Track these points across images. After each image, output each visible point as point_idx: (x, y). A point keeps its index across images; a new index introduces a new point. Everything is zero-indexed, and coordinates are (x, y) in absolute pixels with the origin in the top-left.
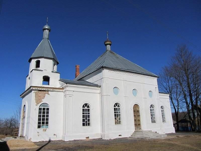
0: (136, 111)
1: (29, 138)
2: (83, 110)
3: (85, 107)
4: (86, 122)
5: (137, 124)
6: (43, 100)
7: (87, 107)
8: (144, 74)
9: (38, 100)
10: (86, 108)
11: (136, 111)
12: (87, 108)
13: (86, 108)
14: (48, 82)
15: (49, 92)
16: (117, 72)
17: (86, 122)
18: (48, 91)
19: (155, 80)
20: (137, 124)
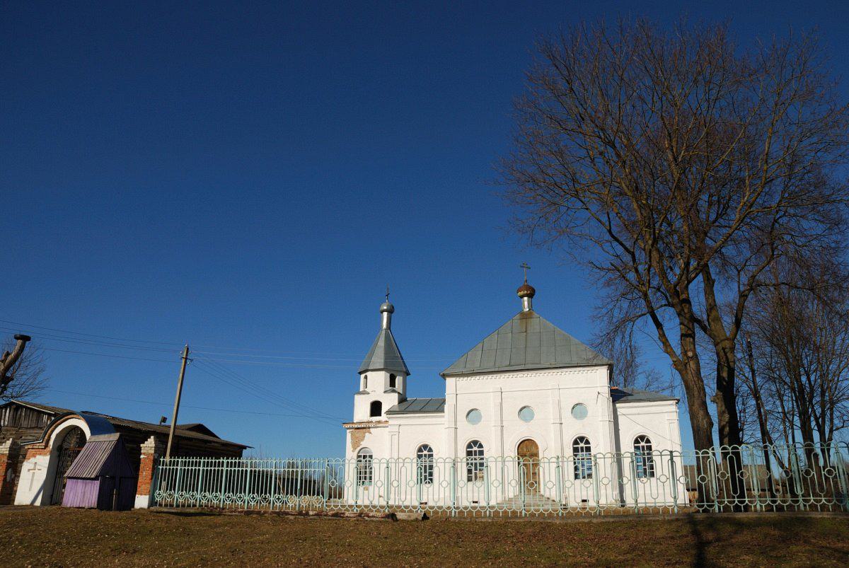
0: (527, 450)
1: (79, 484)
2: (420, 457)
3: (472, 448)
4: (427, 475)
5: (530, 477)
6: (362, 443)
7: (646, 443)
8: (560, 368)
9: (355, 444)
10: (424, 451)
11: (527, 450)
12: (645, 445)
13: (424, 451)
14: (176, 434)
15: (371, 429)
16: (478, 377)
17: (427, 475)
18: (369, 428)
19: (603, 373)
20: (530, 477)
